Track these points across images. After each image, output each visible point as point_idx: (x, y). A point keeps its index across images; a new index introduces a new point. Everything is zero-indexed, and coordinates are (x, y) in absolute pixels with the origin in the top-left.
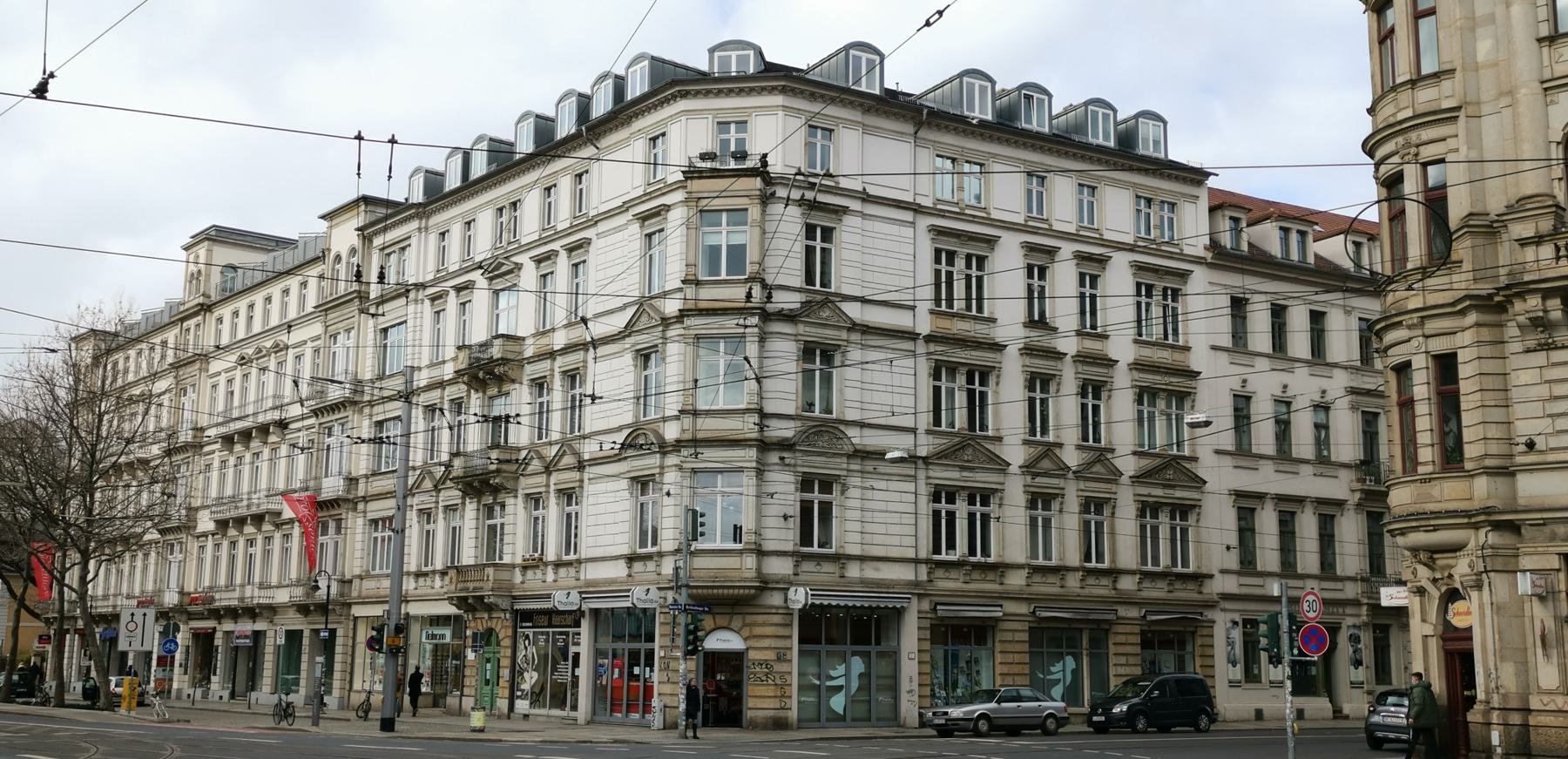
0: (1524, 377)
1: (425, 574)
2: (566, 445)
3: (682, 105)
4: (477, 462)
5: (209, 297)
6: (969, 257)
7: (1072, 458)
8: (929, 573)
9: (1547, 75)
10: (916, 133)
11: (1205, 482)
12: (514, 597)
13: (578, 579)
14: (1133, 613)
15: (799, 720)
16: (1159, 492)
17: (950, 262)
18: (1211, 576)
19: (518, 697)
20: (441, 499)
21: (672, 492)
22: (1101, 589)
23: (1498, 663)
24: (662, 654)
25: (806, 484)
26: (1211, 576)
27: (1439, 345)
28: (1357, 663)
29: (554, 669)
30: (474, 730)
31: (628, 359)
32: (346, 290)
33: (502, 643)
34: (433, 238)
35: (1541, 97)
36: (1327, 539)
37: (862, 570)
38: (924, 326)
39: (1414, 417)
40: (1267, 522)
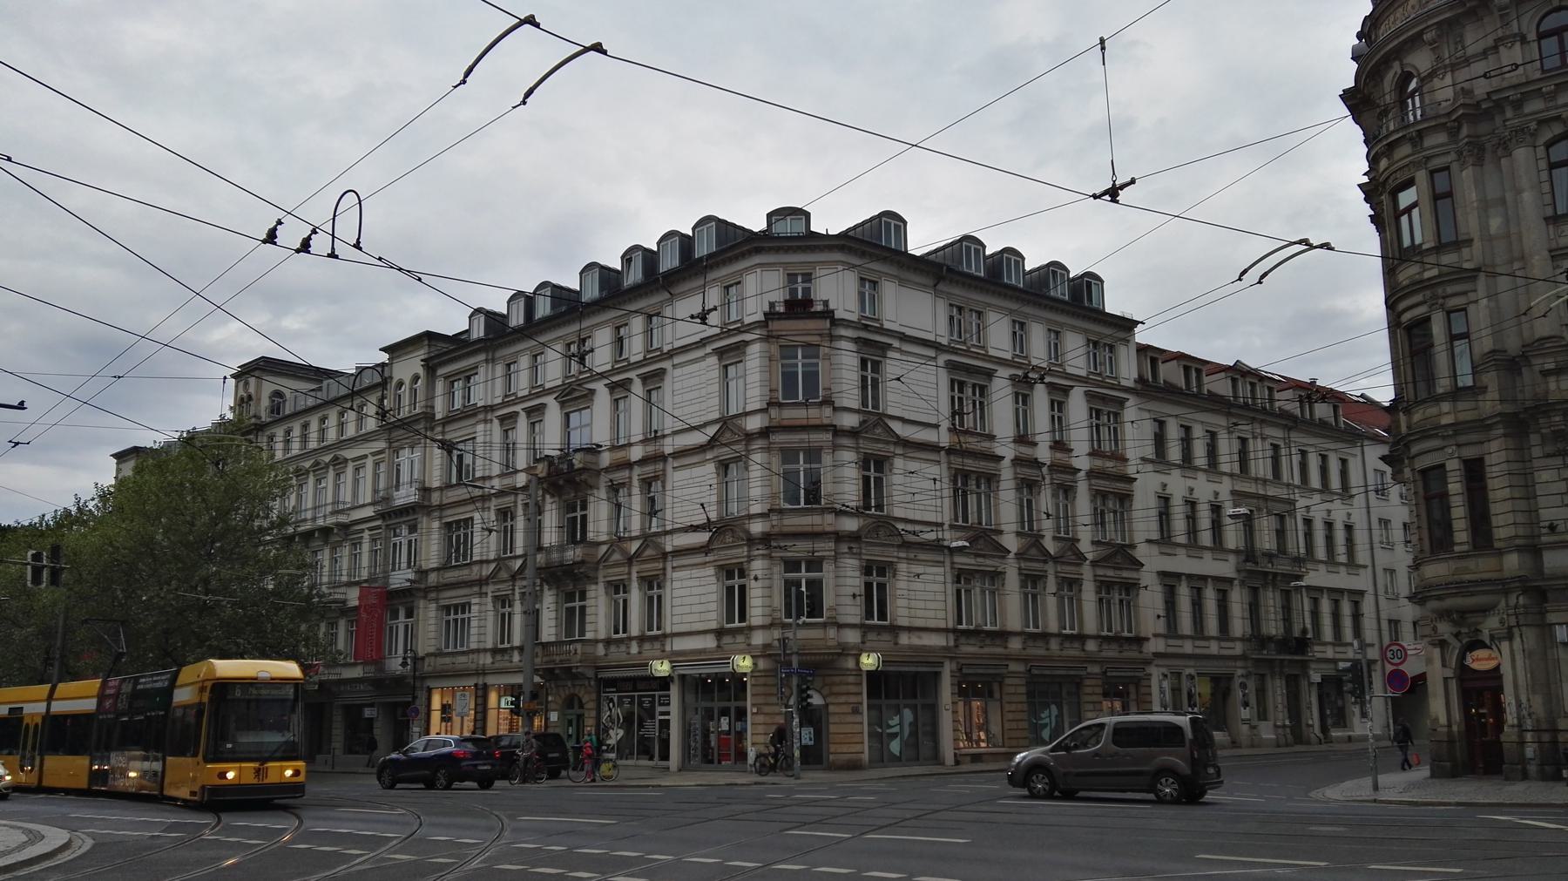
0: (1545, 476)
1: (504, 651)
2: (647, 538)
3: (757, 259)
4: (555, 556)
5: (260, 418)
6: (974, 386)
7: (1050, 546)
8: (956, 640)
9: (1554, 245)
10: (935, 286)
11: (1143, 565)
12: (598, 668)
13: (663, 651)
14: (1095, 669)
15: (870, 761)
16: (1110, 573)
17: (961, 391)
18: (1147, 639)
20: (517, 588)
21: (760, 577)
22: (1073, 651)
23: (1531, 697)
24: (755, 710)
25: (867, 570)
26: (1147, 639)
27: (1470, 452)
28: (1246, 704)
29: (641, 726)
31: (711, 468)
32: (410, 412)
33: (586, 706)
34: (500, 370)
35: (1550, 262)
36: (1197, 605)
37: (909, 638)
38: (944, 439)
39: (1449, 508)
40: (1184, 593)
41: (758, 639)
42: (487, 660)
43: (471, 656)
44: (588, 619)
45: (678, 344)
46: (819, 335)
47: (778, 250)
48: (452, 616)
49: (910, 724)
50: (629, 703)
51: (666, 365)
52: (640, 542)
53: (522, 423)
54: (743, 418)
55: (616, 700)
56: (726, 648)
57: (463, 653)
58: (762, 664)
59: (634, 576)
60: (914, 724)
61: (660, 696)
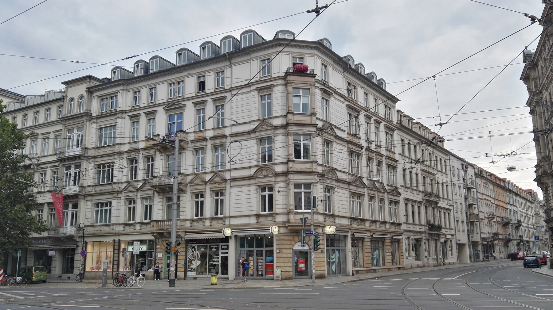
14: (368, 234)
19: (189, 271)
24: (278, 251)
29: (211, 259)
30: (213, 284)
41: (280, 219)
42: (120, 229)
43: (112, 227)
44: (181, 210)
45: (233, 86)
46: (310, 84)
47: (295, 46)
48: (99, 209)
49: (338, 257)
50: (204, 248)
51: (228, 95)
52: (127, 184)
53: (143, 120)
54: (272, 120)
55: (196, 247)
56: (262, 223)
57: (107, 225)
58: (283, 230)
59: (139, 197)
60: (339, 258)
61: (222, 246)
